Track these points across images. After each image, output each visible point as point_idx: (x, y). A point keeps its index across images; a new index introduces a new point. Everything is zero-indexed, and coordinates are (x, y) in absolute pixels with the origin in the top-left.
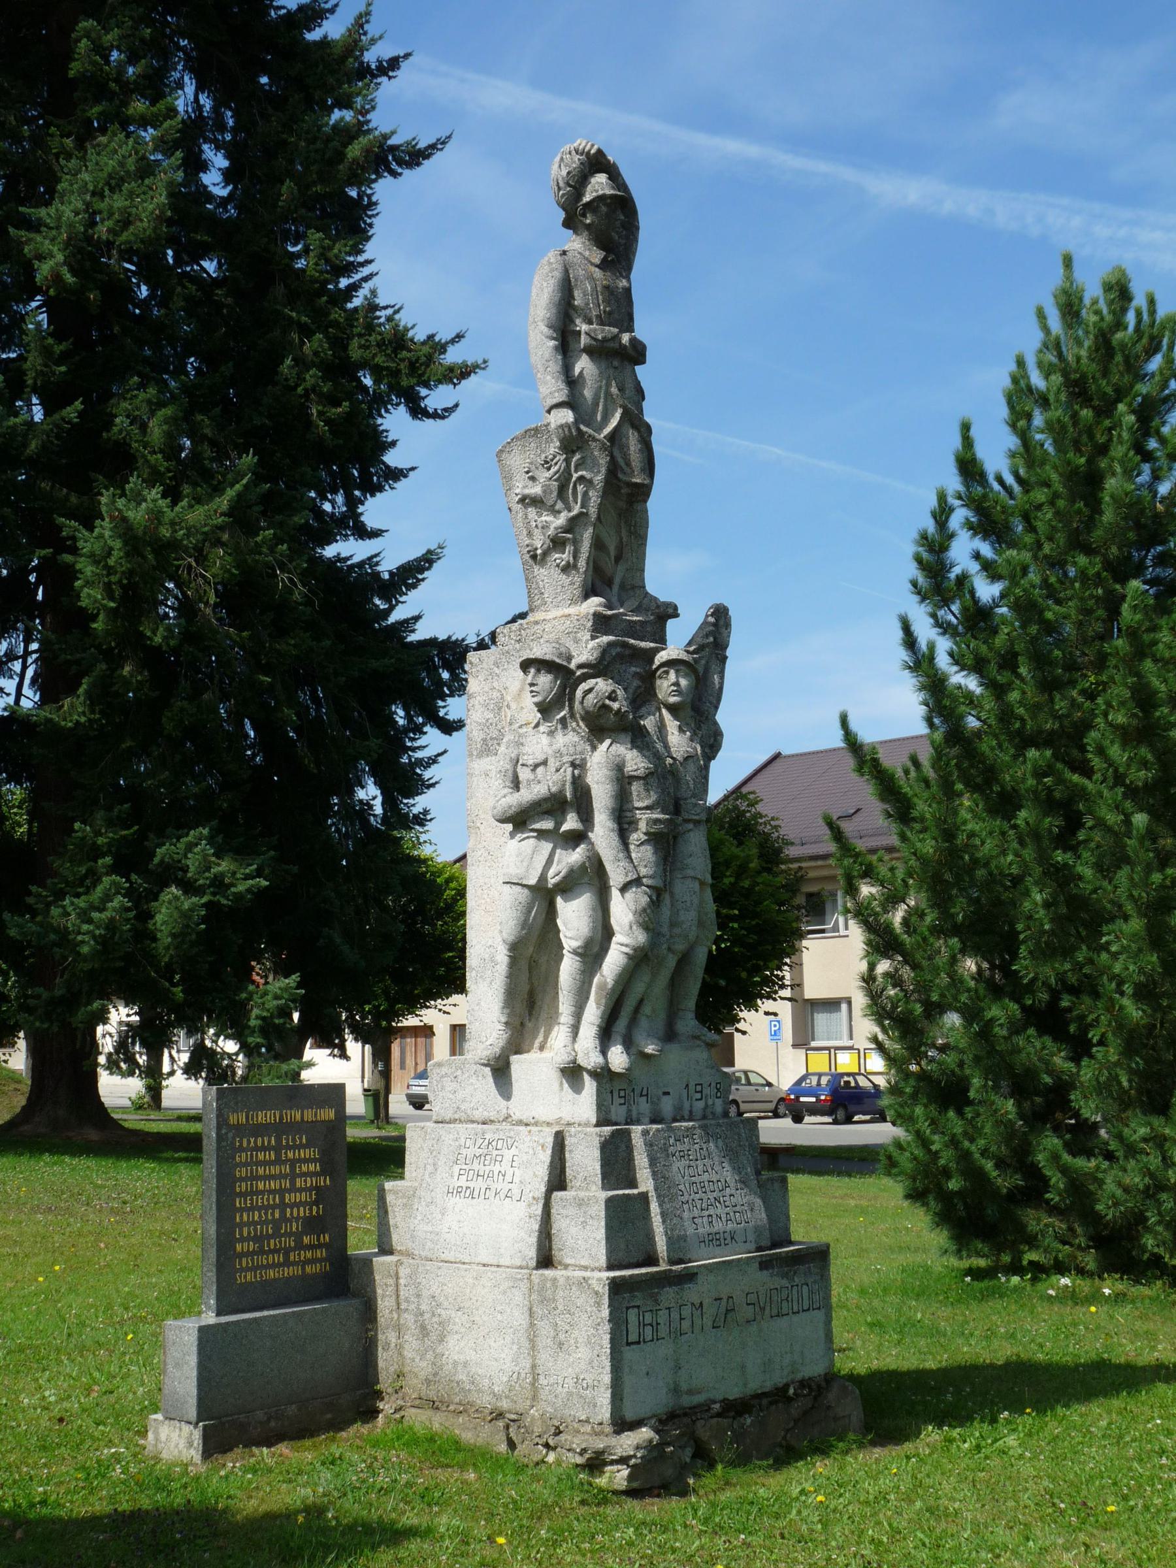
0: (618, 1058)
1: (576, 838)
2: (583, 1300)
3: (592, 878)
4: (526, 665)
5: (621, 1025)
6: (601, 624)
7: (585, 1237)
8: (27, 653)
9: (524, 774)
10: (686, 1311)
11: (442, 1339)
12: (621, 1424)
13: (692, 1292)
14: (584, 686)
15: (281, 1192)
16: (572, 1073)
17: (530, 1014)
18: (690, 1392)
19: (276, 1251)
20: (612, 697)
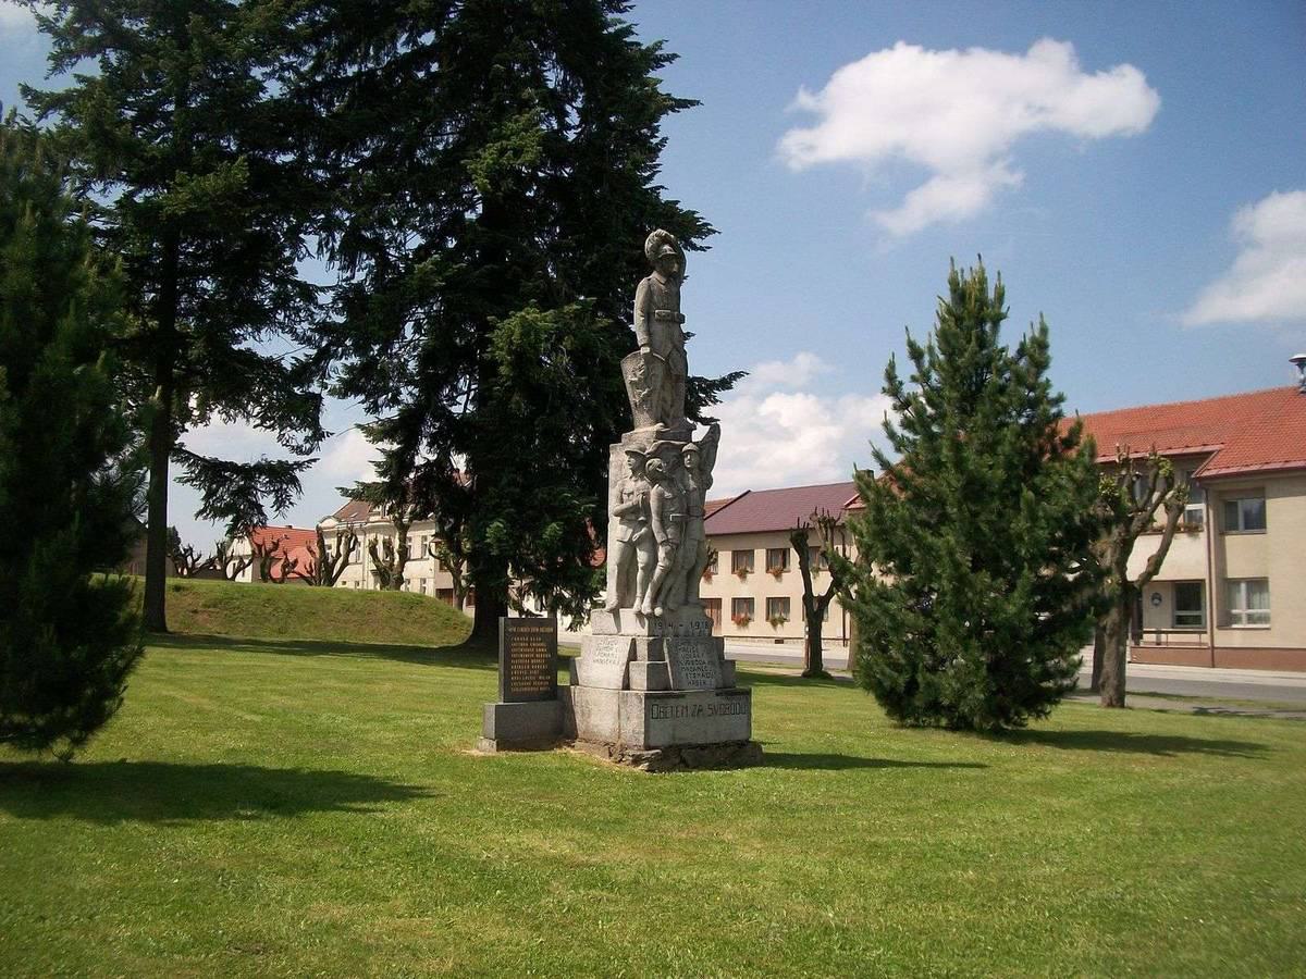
0: (658, 611)
1: (644, 523)
2: (636, 701)
3: (650, 542)
4: (627, 453)
5: (661, 598)
6: (659, 435)
7: (640, 679)
8: (470, 390)
9: (625, 497)
10: (680, 709)
11: (589, 717)
12: (648, 748)
13: (682, 702)
14: (649, 462)
15: (530, 659)
16: (639, 615)
17: (628, 590)
18: (680, 739)
19: (527, 681)
20: (660, 467)
